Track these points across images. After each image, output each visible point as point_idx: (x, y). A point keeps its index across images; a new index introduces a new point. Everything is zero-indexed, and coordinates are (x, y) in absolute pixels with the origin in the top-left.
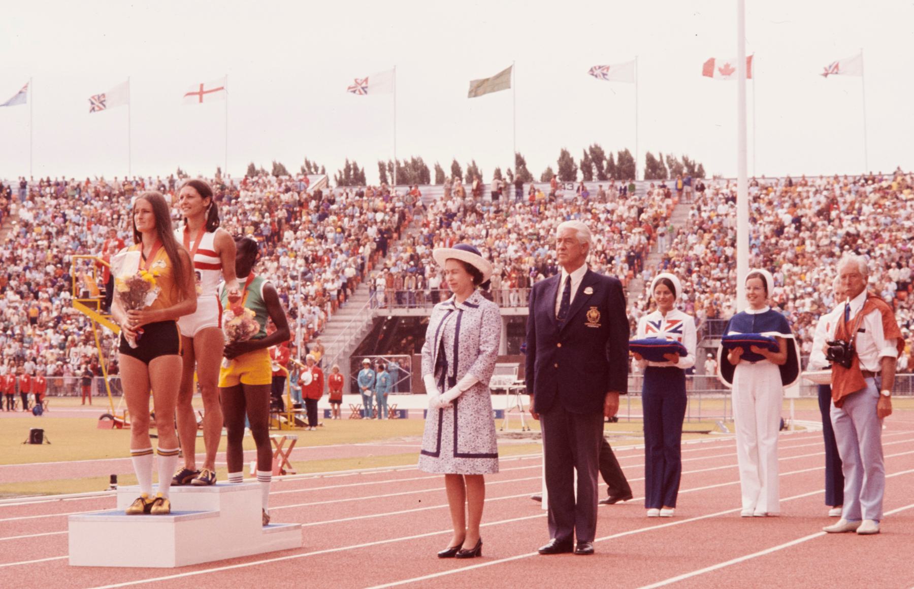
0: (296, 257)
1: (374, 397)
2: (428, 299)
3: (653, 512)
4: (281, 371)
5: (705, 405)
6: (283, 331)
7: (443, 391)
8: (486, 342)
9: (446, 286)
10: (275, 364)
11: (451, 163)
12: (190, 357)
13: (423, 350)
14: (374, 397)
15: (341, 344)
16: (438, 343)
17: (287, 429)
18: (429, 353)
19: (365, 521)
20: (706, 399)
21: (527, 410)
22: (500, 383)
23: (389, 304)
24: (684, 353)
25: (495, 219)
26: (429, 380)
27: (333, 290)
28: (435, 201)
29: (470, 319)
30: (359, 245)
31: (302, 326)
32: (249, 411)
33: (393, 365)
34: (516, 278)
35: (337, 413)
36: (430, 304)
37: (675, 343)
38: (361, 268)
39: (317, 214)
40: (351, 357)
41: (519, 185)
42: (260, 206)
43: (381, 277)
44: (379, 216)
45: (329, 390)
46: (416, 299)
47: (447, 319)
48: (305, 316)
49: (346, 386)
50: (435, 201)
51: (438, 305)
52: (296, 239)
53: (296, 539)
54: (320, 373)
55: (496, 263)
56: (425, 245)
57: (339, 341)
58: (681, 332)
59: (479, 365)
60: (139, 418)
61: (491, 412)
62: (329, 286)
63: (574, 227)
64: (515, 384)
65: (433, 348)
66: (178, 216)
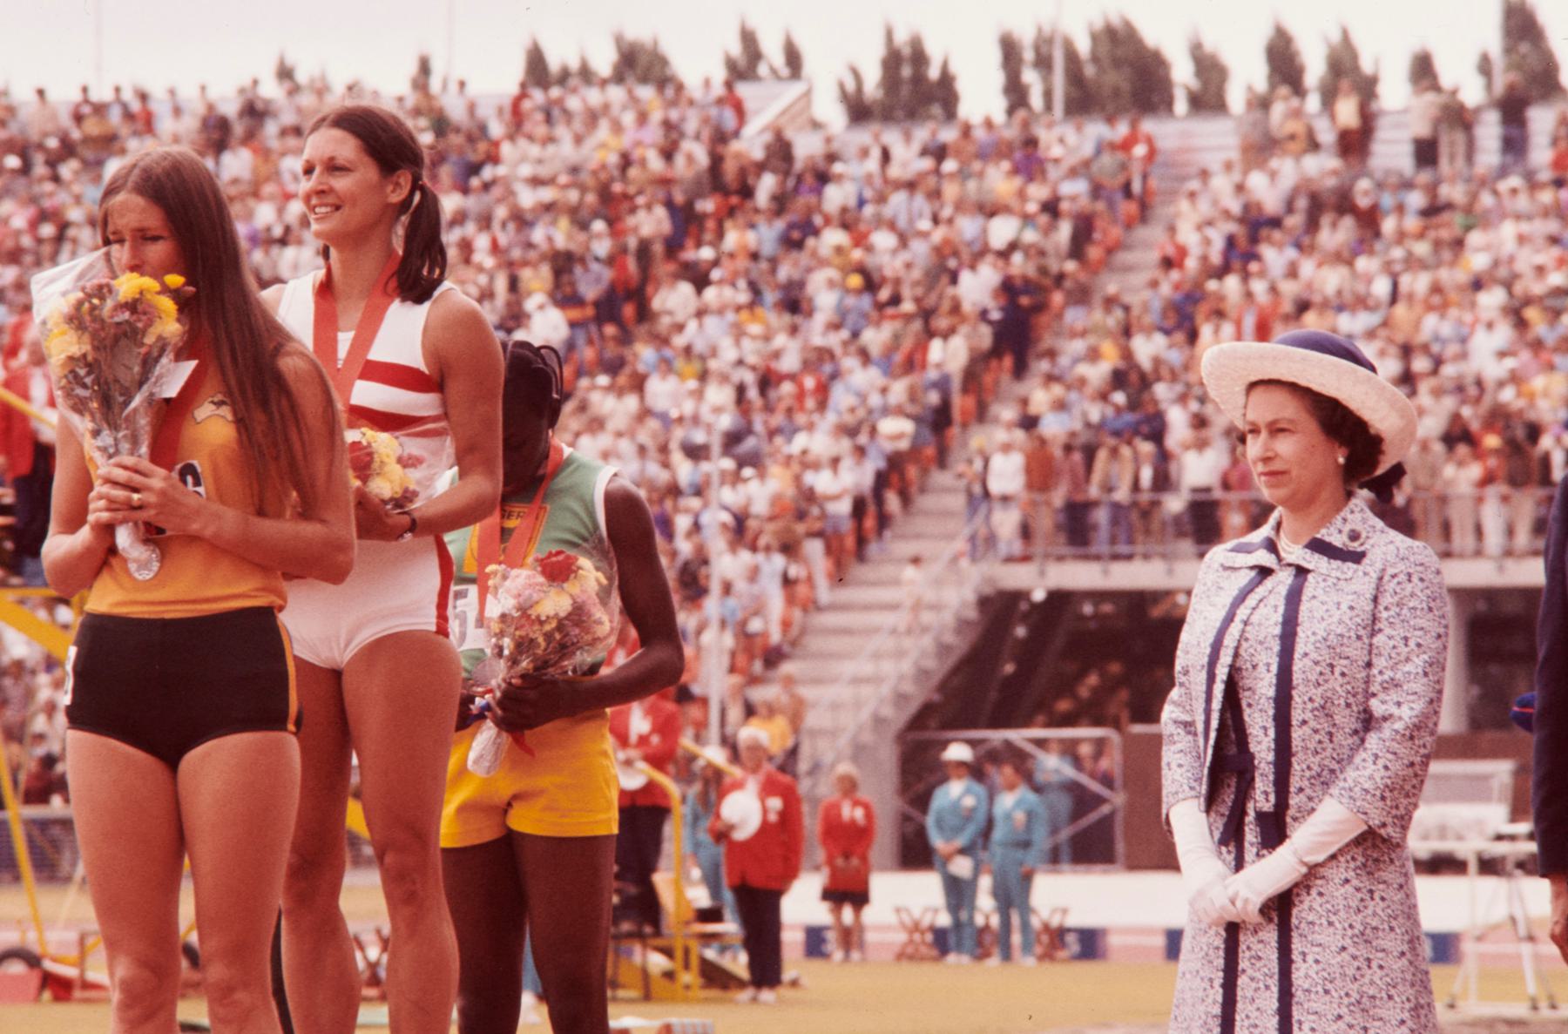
0: (703, 376)
1: (985, 882)
2: (1179, 527)
4: (651, 787)
6: (660, 654)
7: (1239, 865)
9: (1245, 482)
10: (628, 763)
11: (1260, 37)
12: (333, 733)
13: (1168, 712)
14: (985, 882)
16: (1219, 689)
17: (671, 999)
18: (1188, 726)
21: (1544, 933)
22: (1443, 832)
23: (1039, 547)
25: (1421, 235)
26: (1189, 823)
27: (836, 498)
28: (1204, 175)
29: (1333, 600)
30: (930, 333)
31: (723, 624)
33: (1052, 765)
34: (1496, 452)
35: (850, 938)
36: (1187, 546)
38: (939, 421)
39: (780, 225)
40: (901, 737)
41: (1513, 109)
42: (573, 196)
43: (1006, 448)
44: (1002, 231)
45: (820, 854)
46: (1137, 524)
47: (1251, 601)
48: (741, 588)
49: (884, 841)
50: (1204, 175)
51: (1218, 553)
52: (700, 313)
54: (791, 800)
55: (1424, 397)
56: (1167, 332)
57: (857, 681)
59: (1369, 769)
60: (144, 963)
61: (1413, 941)
62: (822, 482)
64: (1500, 838)
65: (1200, 706)
66: (278, 232)
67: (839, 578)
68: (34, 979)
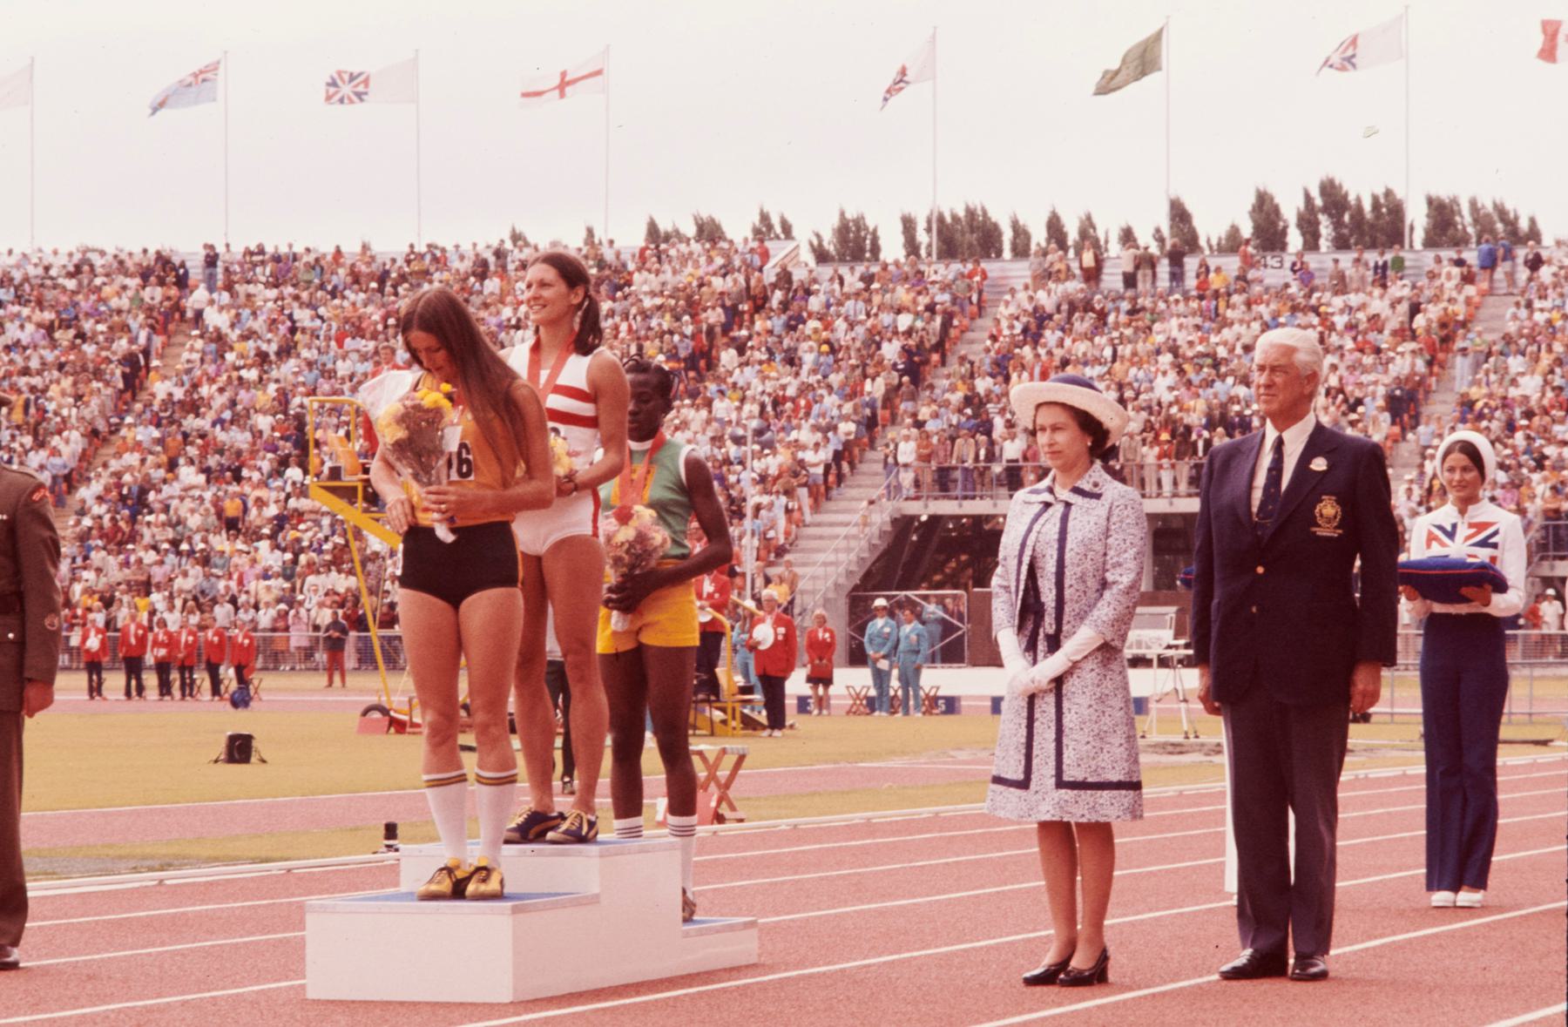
3: (1442, 897)
5: (1540, 690)
8: (1120, 565)
15: (831, 569)
19: (881, 913)
20: (1542, 678)
24: (1501, 586)
32: (655, 700)
35: (822, 702)
37: (1483, 566)
53: (745, 948)
57: (825, 564)
58: (1495, 546)
63: (1291, 342)
67: (816, 508)
68: (386, 721)
